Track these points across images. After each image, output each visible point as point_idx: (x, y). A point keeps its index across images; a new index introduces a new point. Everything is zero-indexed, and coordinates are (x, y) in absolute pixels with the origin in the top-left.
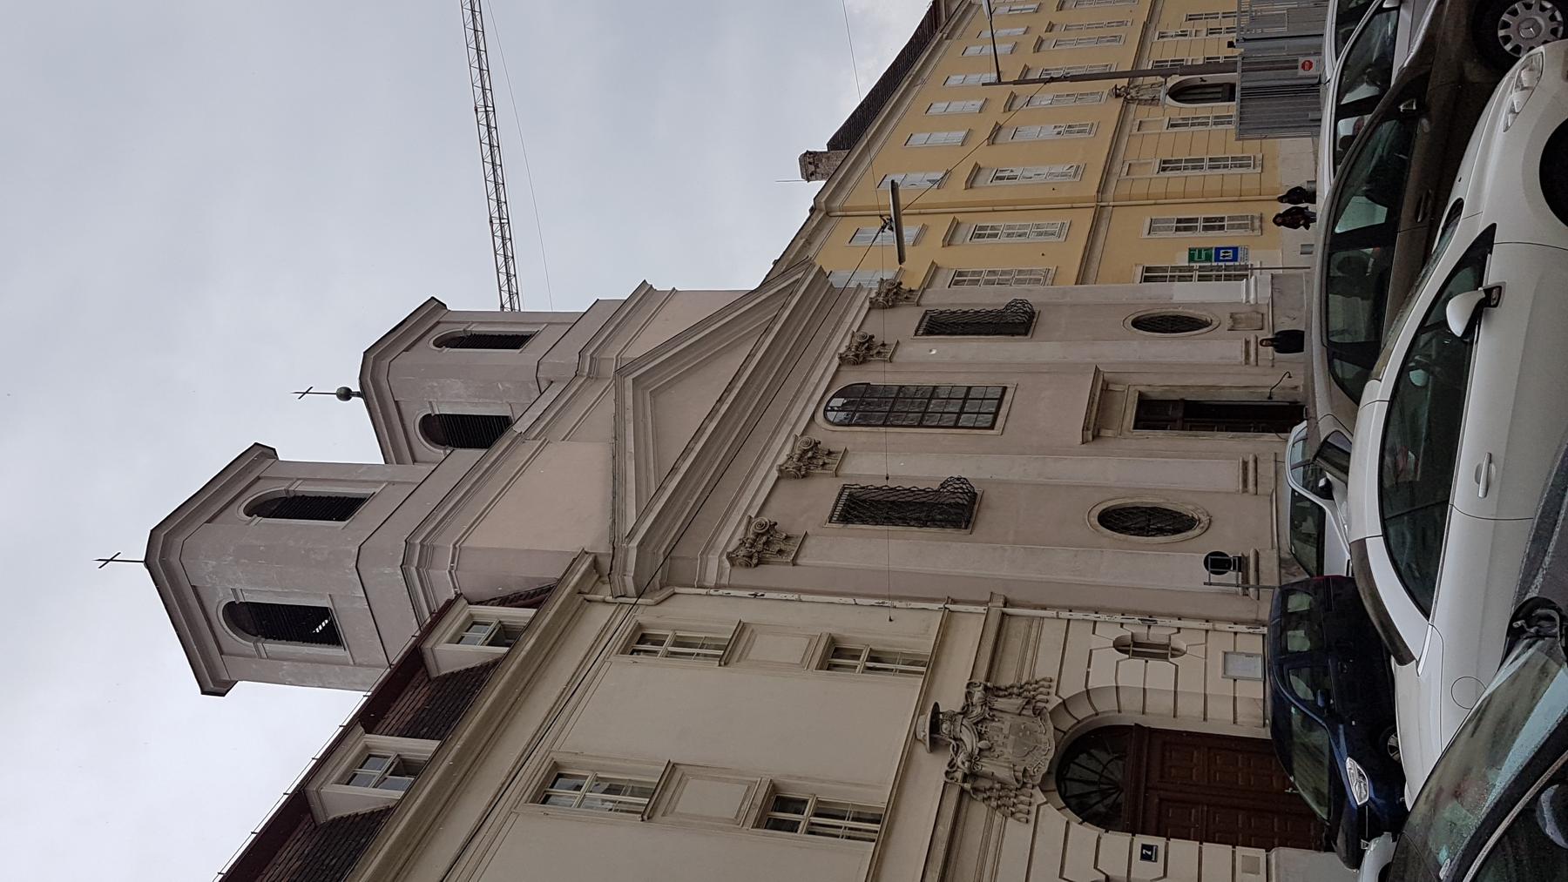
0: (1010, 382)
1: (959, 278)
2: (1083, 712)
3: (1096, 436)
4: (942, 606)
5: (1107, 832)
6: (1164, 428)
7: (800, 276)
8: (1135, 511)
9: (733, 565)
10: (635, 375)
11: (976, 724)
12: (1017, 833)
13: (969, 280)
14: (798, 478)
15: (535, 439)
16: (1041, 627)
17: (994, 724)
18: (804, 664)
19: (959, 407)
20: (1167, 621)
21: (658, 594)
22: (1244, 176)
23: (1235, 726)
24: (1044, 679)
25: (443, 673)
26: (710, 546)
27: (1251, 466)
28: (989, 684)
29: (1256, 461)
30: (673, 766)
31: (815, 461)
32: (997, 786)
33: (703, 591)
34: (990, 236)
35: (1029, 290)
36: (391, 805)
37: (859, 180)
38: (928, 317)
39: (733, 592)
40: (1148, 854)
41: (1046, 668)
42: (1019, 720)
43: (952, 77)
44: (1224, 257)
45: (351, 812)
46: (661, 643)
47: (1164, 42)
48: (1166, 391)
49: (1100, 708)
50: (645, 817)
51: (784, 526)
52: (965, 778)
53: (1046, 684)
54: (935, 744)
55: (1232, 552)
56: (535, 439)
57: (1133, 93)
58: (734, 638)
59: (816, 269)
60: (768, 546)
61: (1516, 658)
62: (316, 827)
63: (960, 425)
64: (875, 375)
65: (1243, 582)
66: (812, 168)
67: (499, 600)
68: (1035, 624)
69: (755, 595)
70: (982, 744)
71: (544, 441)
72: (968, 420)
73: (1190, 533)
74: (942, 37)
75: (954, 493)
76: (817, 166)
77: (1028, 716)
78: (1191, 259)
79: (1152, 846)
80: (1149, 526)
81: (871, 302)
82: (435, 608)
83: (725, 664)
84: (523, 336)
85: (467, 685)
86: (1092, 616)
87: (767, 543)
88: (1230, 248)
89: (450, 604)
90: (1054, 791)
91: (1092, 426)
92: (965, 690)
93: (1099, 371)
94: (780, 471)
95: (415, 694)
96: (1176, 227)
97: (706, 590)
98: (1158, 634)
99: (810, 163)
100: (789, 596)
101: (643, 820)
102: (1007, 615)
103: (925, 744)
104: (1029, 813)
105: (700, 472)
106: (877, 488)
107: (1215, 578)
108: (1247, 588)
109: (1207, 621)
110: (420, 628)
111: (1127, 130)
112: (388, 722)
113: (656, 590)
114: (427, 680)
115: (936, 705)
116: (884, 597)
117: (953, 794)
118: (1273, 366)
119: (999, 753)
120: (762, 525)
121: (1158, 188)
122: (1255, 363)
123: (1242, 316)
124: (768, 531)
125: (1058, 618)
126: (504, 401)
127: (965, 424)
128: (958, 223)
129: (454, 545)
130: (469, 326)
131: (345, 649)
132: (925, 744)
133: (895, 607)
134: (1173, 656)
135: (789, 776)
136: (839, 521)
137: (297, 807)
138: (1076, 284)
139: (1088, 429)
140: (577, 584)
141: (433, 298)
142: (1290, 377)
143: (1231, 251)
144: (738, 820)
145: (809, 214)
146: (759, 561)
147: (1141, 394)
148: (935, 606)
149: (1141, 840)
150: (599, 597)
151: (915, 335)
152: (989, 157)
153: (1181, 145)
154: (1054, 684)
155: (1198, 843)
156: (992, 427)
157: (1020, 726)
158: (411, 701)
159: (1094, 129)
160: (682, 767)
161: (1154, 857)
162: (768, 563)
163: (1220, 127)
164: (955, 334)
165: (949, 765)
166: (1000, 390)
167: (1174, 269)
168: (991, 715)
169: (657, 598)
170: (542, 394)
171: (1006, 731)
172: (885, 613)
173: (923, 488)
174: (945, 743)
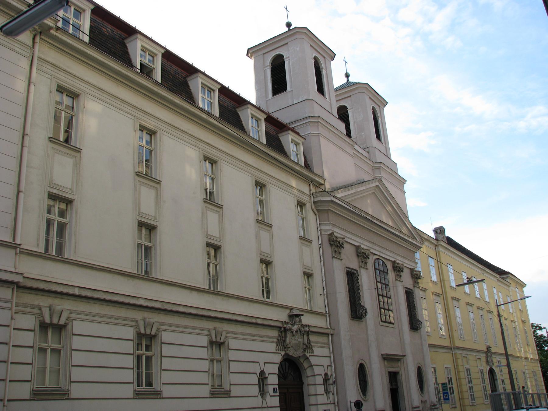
2: (306, 365)
3: (384, 359)
4: (328, 312)
7: (418, 240)
9: (329, 235)
10: (379, 185)
11: (299, 330)
12: (272, 347)
14: (357, 253)
16: (326, 348)
17: (300, 335)
18: (304, 267)
20: (335, 390)
24: (313, 351)
25: (280, 138)
26: (334, 225)
28: (310, 332)
30: (159, 183)
31: (363, 258)
32: (284, 339)
36: (247, 133)
37: (454, 259)
38: (411, 291)
39: (320, 236)
40: (275, 390)
41: (317, 351)
43: (485, 284)
44: (447, 396)
45: (242, 120)
47: (497, 362)
50: (205, 200)
51: (343, 251)
52: (285, 328)
54: (291, 316)
57: (489, 354)
58: (306, 239)
59: (421, 246)
62: (235, 108)
66: (439, 231)
68: (327, 346)
69: (320, 245)
70: (294, 332)
71: (353, 156)
74: (498, 278)
76: (440, 233)
77: (303, 347)
82: (295, 129)
83: (257, 222)
84: (324, 93)
86: (333, 365)
87: (338, 246)
92: (307, 324)
93: (404, 357)
94: (359, 246)
96: (449, 377)
98: (331, 388)
99: (441, 231)
100: (322, 257)
101: (203, 199)
103: (290, 312)
104: (279, 350)
105: (355, 217)
107: (353, 404)
111: (477, 354)
114: (235, 107)
115: (303, 315)
117: (279, 324)
120: (402, 268)
121: (461, 369)
124: (341, 246)
125: (330, 353)
126: (357, 136)
127: (385, 312)
128: (440, 296)
129: (319, 133)
130: (325, 70)
136: (347, 271)
137: (192, 70)
138: (428, 344)
139: (387, 356)
140: (315, 180)
141: (387, 103)
143: (448, 397)
144: (208, 236)
150: (312, 188)
152: (462, 303)
153: (476, 375)
154: (312, 354)
158: (228, 102)
159: (462, 339)
160: (221, 211)
163: (468, 389)
165: (287, 322)
170: (363, 149)
172: (322, 293)
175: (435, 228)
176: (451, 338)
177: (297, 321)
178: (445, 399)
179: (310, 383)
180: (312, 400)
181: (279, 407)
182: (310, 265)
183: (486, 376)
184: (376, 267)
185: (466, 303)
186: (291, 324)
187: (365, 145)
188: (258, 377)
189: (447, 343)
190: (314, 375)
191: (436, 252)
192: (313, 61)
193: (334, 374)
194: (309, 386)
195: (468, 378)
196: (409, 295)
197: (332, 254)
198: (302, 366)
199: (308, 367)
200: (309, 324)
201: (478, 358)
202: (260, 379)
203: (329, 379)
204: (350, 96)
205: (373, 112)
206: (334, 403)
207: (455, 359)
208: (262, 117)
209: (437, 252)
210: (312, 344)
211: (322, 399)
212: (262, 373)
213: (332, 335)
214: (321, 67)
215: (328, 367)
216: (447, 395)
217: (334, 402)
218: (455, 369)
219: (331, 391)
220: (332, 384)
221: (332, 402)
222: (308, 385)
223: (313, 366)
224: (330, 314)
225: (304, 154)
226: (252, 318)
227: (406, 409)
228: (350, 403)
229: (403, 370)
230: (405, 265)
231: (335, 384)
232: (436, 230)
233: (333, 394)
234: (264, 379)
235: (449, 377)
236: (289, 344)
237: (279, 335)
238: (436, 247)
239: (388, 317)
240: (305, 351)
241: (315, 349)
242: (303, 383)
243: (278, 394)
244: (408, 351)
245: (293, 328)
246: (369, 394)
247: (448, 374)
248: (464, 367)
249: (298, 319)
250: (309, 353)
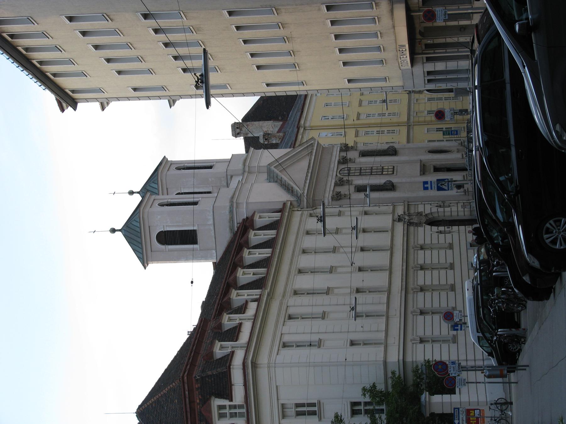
2: (430, 216)
3: (424, 174)
20: (448, 202)
44: (454, 133)
49: (434, 216)
61: (516, 176)
66: (238, 131)
69: (340, 206)
76: (241, 130)
86: (430, 202)
88: (455, 131)
91: (422, 170)
99: (237, 128)
103: (396, 221)
107: (459, 191)
111: (412, 102)
117: (406, 225)
143: (455, 131)
147: (434, 166)
175: (233, 135)
176: (399, 124)
178: (457, 134)
180: (455, 214)
181: (459, 227)
183: (435, 95)
185: (359, 106)
187: (222, 179)
190: (438, 212)
191: (311, 129)
193: (436, 202)
196: (364, 154)
197: (348, 199)
199: (432, 215)
201: (417, 101)
203: (440, 205)
204: (167, 188)
207: (419, 123)
209: (311, 128)
211: (454, 209)
213: (408, 202)
218: (428, 124)
220: (444, 204)
222: (444, 216)
223: (432, 212)
224: (393, 203)
225: (273, 213)
228: (457, 192)
229: (432, 163)
231: (443, 202)
232: (235, 134)
233: (451, 203)
239: (390, 170)
241: (420, 211)
242: (443, 220)
243: (451, 227)
247: (434, 131)
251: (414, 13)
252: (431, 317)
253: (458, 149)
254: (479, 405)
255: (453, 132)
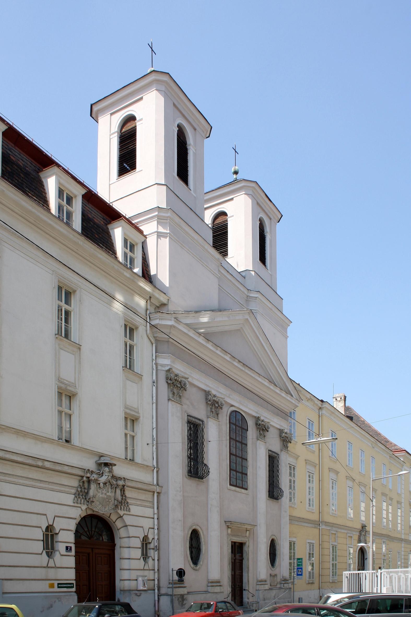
0: (250, 491)
1: (292, 468)
2: (119, 524)
5: (74, 534)
6: (232, 552)
8: (199, 543)
11: (109, 482)
12: (69, 499)
13: (291, 472)
15: (219, 271)
17: (110, 489)
19: (234, 457)
21: (152, 336)
22: (329, 576)
23: (119, 580)
27: (218, 584)
29: (220, 586)
31: (214, 408)
32: (86, 491)
33: (154, 358)
34: (309, 480)
35: (287, 498)
38: (276, 455)
39: (154, 372)
40: (68, 549)
41: (134, 510)
42: (113, 499)
44: (300, 572)
46: (130, 339)
48: (247, 553)
51: (186, 394)
53: (128, 510)
55: (185, 578)
56: (219, 271)
59: (297, 404)
60: (176, 387)
63: (231, 471)
64: (252, 433)
65: (174, 582)
67: (144, 257)
69: (154, 382)
70: (102, 485)
72: (233, 475)
73: (191, 563)
75: (203, 470)
78: (298, 559)
79: (71, 550)
80: (193, 548)
81: (283, 430)
84: (265, 262)
85: (106, 245)
86: (156, 527)
89: (141, 232)
90: (87, 513)
95: (100, 218)
96: (310, 553)
97: (155, 359)
98: (151, 553)
99: (341, 398)
102: (154, 494)
104: (77, 503)
106: (203, 436)
108: (172, 584)
109: (158, 570)
110: (129, 218)
112: (87, 205)
113: (153, 335)
115: (115, 465)
116: (157, 441)
117: (81, 473)
118: (256, 590)
119: (99, 491)
120: (268, 428)
121: (326, 545)
122: (257, 584)
123: (276, 579)
124: (182, 387)
125: (154, 514)
127: (232, 473)
131: (117, 179)
132: (99, 460)
133: (153, 446)
134: (143, 558)
135: (80, 401)
142: (252, 596)
143: (301, 573)
144: (59, 380)
145: (320, 400)
146: (169, 383)
147: (245, 543)
148: (155, 464)
149: (73, 546)
151: (269, 450)
154: (128, 513)
155: (75, 567)
156: (230, 485)
157: (111, 499)
161: (68, 551)
162: (168, 388)
163: (331, 566)
164: (269, 468)
166: (246, 488)
167: (294, 553)
168: (114, 487)
169: (150, 335)
171: (108, 494)
172: (150, 442)
173: (204, 456)
174: (100, 468)
177: (105, 471)
178: (298, 575)
179: (123, 545)
182: (136, 407)
184: (231, 421)
186: (98, 474)
188: (43, 532)
189: (315, 517)
192: (176, 129)
193: (156, 537)
194: (121, 548)
195: (333, 555)
198: (115, 526)
200: (126, 477)
201: (349, 536)
202: (144, 543)
205: (260, 224)
206: (154, 570)
208: (79, 192)
209: (320, 415)
210: (129, 501)
212: (49, 528)
214: (188, 143)
215: (150, 529)
216: (300, 571)
217: (154, 569)
218: (320, 545)
219: (151, 557)
220: (153, 549)
221: (150, 569)
222: (120, 547)
226: (36, 459)
227: (248, 581)
228: (172, 571)
230: (272, 423)
231: (157, 549)
234: (54, 535)
235: (310, 553)
236: (93, 497)
237: (80, 485)
238: (320, 410)
240: (118, 507)
242: (115, 545)
244: (261, 521)
245: (100, 479)
246: (201, 563)
247: (310, 549)
248: (348, 546)
249: (107, 469)
250: (124, 510)
251: (75, 201)
252: (72, 529)
253: (276, 575)
254: (168, 588)
255: (301, 570)
